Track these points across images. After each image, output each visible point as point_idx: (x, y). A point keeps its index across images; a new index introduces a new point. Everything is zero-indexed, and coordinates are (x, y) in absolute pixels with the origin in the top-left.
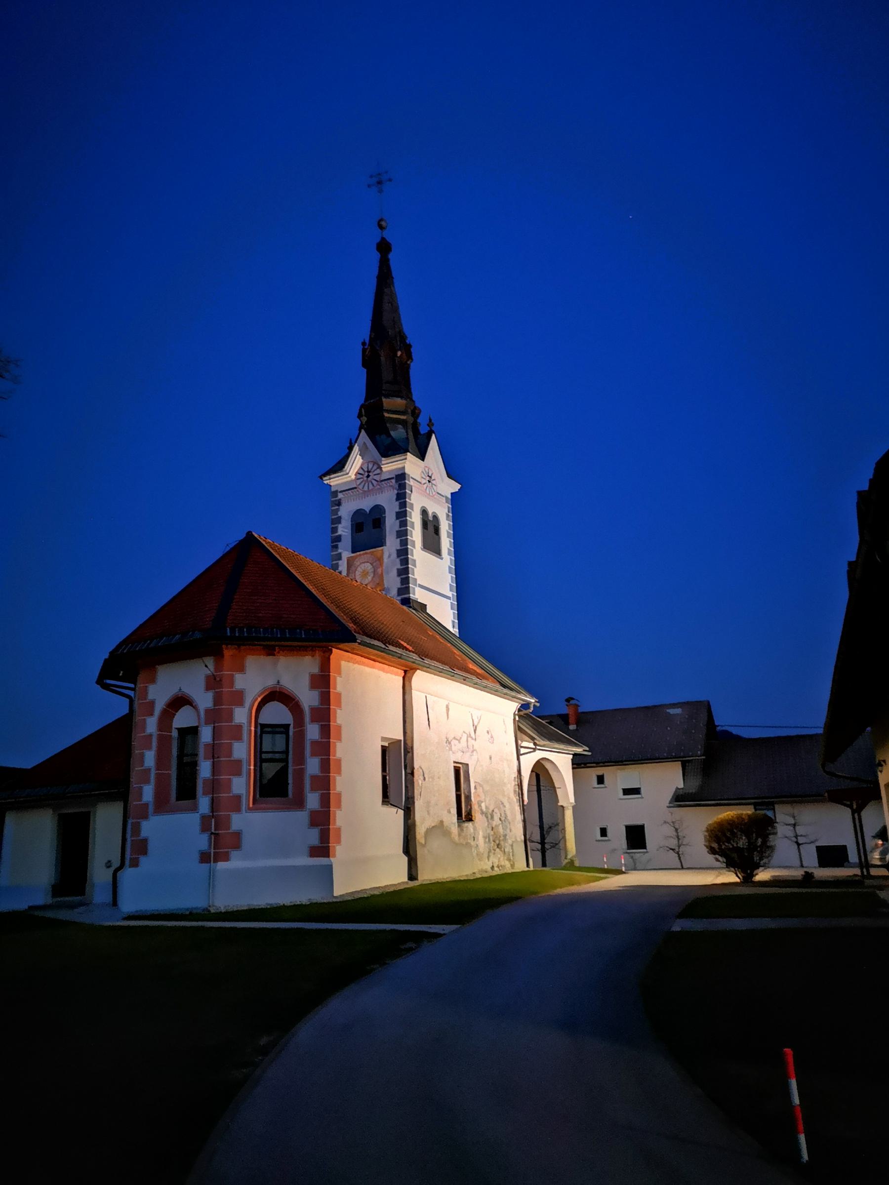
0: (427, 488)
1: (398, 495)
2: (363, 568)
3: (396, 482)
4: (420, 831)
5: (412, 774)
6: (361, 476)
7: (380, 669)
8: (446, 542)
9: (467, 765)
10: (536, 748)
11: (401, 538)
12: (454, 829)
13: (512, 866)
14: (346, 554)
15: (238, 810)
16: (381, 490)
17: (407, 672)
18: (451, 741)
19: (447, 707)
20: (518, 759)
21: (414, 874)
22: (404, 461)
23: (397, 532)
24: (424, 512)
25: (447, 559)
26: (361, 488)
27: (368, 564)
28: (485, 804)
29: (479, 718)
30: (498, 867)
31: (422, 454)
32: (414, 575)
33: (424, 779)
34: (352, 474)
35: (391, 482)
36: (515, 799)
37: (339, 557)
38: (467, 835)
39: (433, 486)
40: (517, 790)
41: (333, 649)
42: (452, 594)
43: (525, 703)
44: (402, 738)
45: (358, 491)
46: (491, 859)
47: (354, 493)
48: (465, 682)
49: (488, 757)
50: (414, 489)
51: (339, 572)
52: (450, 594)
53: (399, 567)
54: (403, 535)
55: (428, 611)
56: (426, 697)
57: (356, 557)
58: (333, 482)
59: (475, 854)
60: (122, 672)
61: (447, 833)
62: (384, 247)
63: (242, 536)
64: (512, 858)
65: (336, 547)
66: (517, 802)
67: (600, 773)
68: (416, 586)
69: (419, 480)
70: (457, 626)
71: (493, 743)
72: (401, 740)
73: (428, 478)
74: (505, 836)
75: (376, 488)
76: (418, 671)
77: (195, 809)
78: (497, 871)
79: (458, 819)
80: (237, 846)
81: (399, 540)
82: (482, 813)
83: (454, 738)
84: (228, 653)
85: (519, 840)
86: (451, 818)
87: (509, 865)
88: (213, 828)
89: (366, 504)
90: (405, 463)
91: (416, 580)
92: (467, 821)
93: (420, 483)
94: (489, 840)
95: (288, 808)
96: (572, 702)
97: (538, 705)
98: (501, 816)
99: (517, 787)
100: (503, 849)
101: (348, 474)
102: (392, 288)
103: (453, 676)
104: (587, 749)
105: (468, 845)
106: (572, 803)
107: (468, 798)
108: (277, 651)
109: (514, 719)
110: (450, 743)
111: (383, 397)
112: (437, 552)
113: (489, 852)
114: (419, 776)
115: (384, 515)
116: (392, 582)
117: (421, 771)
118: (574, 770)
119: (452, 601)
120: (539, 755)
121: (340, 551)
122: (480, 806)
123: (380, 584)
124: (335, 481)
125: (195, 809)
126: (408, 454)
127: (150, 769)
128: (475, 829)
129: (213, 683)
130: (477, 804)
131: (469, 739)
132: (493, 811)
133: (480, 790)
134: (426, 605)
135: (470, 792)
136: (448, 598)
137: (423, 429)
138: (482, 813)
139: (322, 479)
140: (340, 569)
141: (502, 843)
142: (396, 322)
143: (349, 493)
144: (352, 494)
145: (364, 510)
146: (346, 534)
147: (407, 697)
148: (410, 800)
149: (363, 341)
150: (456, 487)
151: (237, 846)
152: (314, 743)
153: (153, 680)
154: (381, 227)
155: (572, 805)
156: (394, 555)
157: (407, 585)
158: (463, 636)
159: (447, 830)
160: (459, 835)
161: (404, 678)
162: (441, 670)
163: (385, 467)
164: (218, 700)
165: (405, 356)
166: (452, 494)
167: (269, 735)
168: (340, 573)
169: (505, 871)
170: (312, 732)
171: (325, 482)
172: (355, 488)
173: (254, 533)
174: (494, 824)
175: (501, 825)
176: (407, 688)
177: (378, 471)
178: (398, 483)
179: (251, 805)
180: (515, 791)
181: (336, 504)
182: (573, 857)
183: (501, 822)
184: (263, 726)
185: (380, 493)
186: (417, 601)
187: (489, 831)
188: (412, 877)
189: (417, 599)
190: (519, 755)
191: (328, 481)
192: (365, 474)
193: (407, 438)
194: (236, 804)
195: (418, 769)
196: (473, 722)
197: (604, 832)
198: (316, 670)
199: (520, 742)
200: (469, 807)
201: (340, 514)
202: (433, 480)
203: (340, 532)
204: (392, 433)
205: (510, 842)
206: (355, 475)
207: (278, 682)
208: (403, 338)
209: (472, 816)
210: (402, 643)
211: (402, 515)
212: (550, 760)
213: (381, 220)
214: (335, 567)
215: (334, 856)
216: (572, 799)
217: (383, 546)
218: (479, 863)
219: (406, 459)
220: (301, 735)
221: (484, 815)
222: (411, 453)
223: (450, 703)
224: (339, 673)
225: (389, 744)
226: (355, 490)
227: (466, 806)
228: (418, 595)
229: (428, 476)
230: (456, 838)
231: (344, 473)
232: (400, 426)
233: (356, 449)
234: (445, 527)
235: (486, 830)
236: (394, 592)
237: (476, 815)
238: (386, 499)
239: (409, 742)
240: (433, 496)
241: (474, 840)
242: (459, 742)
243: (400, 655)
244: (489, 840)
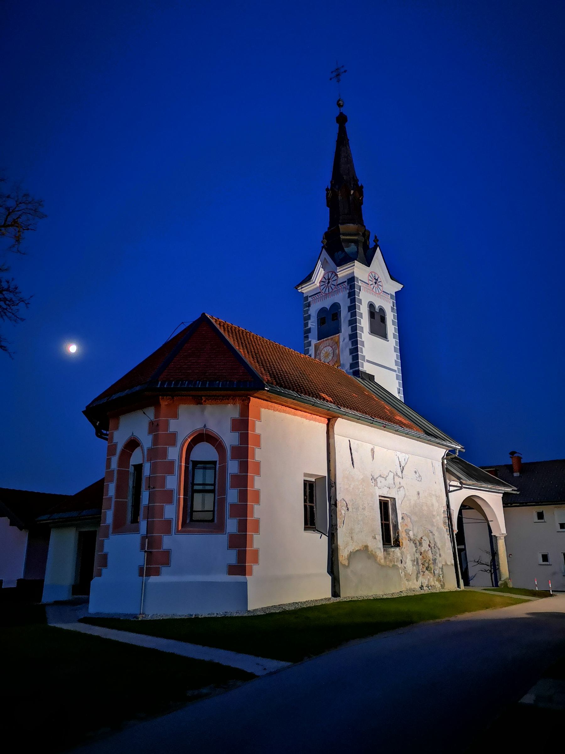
0: (373, 287)
1: (349, 293)
2: (326, 351)
3: (348, 284)
4: (343, 554)
5: (336, 505)
6: (324, 283)
7: (302, 416)
8: (391, 329)
9: (395, 499)
10: (462, 486)
11: (352, 326)
12: (380, 554)
13: (443, 586)
14: (314, 342)
15: (168, 532)
16: (338, 292)
17: (331, 420)
18: (377, 478)
19: (373, 450)
20: (447, 496)
21: (337, 591)
22: (353, 267)
23: (349, 321)
24: (371, 306)
25: (392, 342)
26: (324, 292)
27: (330, 347)
28: (413, 532)
29: (406, 461)
30: (427, 586)
31: (368, 262)
32: (362, 353)
33: (348, 509)
34: (317, 283)
35: (344, 284)
36: (444, 529)
37: (309, 344)
38: (394, 559)
39: (379, 286)
40: (447, 521)
41: (251, 398)
42: (397, 368)
43: (451, 449)
44: (326, 475)
45: (321, 294)
46: (421, 579)
47: (319, 296)
48: (385, 428)
49: (416, 493)
51: (309, 355)
52: (395, 368)
53: (351, 347)
54: (353, 323)
55: (375, 381)
56: (349, 440)
57: (320, 343)
58: (303, 290)
59: (403, 575)
60: (98, 422)
61: (372, 556)
62: (342, 119)
63: (197, 316)
64: (442, 580)
65: (307, 337)
66: (447, 531)
67: (540, 511)
68: (365, 361)
70: (402, 392)
71: (421, 481)
72: (326, 476)
73: (374, 281)
74: (435, 560)
75: (334, 290)
76: (339, 418)
77: (137, 530)
78: (426, 590)
79: (383, 544)
80: (167, 563)
81: (350, 327)
82: (410, 540)
83: (380, 476)
84: (164, 403)
85: (449, 563)
86: (377, 544)
87: (439, 586)
88: (146, 549)
89: (327, 303)
90: (354, 268)
91: (364, 356)
92: (395, 546)
93: (368, 284)
94: (417, 563)
95: (211, 532)
96: (516, 455)
97: (464, 450)
98: (430, 542)
99: (447, 519)
100: (432, 572)
101: (314, 283)
102: (348, 147)
103: (372, 423)
104: (516, 489)
105: (395, 567)
106: (503, 534)
107: (396, 527)
108: (204, 400)
109: (443, 463)
110: (375, 480)
111: (339, 225)
112: (384, 336)
113: (417, 574)
114: (341, 507)
116: (346, 359)
117: (344, 502)
118: (504, 508)
119: (397, 373)
120: (465, 493)
121: (310, 339)
122: (407, 533)
123: (338, 361)
124: (306, 289)
125: (137, 530)
126: (356, 261)
127: (112, 497)
128: (402, 553)
129: (154, 427)
130: (404, 532)
131: (396, 477)
133: (407, 520)
134: (374, 376)
135: (397, 522)
136: (395, 371)
137: (371, 244)
138: (410, 540)
139: (297, 288)
140: (310, 353)
141: (432, 566)
142: (351, 171)
143: (315, 296)
144: (317, 297)
145: (326, 308)
146: (314, 327)
147: (331, 441)
148: (334, 527)
149: (327, 187)
150: (399, 287)
151: (167, 563)
152: (234, 476)
153: (117, 428)
154: (339, 105)
155: (504, 535)
156: (347, 339)
157: (357, 361)
158: (407, 402)
159: (372, 554)
160: (385, 558)
161: (328, 425)
162: (359, 418)
163: (340, 274)
164: (156, 441)
165: (357, 194)
166: (395, 292)
168: (310, 356)
169: (434, 591)
170: (233, 467)
171: (299, 291)
172: (320, 292)
173: (206, 314)
174: (423, 550)
175: (430, 551)
176: (331, 433)
177: (336, 277)
178: (349, 285)
179: (180, 528)
180: (445, 523)
181: (306, 306)
182: (507, 579)
183: (430, 548)
184: (195, 463)
185: (337, 294)
186: (366, 373)
187: (418, 555)
188: (335, 593)
189: (366, 371)
190: (447, 492)
191: (301, 290)
192: (326, 281)
193: (358, 252)
194: (167, 526)
195: (341, 501)
196: (400, 463)
197: (545, 558)
198: (236, 414)
199: (448, 481)
200: (397, 535)
201: (309, 313)
202: (379, 282)
203: (310, 326)
204: (346, 249)
205: (440, 565)
206: (320, 283)
207: (205, 426)
208: (356, 181)
209: (399, 542)
210: (323, 395)
211: (353, 309)
212: (481, 498)
213: (339, 100)
214: (306, 352)
215: (251, 574)
216: (504, 531)
217: (339, 333)
218: (406, 582)
219: (354, 265)
220: (224, 469)
221: (412, 542)
222: (358, 261)
223: (375, 446)
224: (259, 418)
225: (315, 479)
226: (320, 294)
227: (394, 533)
228: (366, 368)
229: (375, 279)
230: (382, 561)
231: (311, 282)
232: (353, 244)
233: (319, 263)
234: (391, 317)
235: (414, 555)
236: (348, 366)
237: (403, 541)
238: (341, 298)
239: (333, 479)
240: (379, 294)
241: (402, 563)
242: (386, 480)
243: (313, 403)
244: (417, 563)
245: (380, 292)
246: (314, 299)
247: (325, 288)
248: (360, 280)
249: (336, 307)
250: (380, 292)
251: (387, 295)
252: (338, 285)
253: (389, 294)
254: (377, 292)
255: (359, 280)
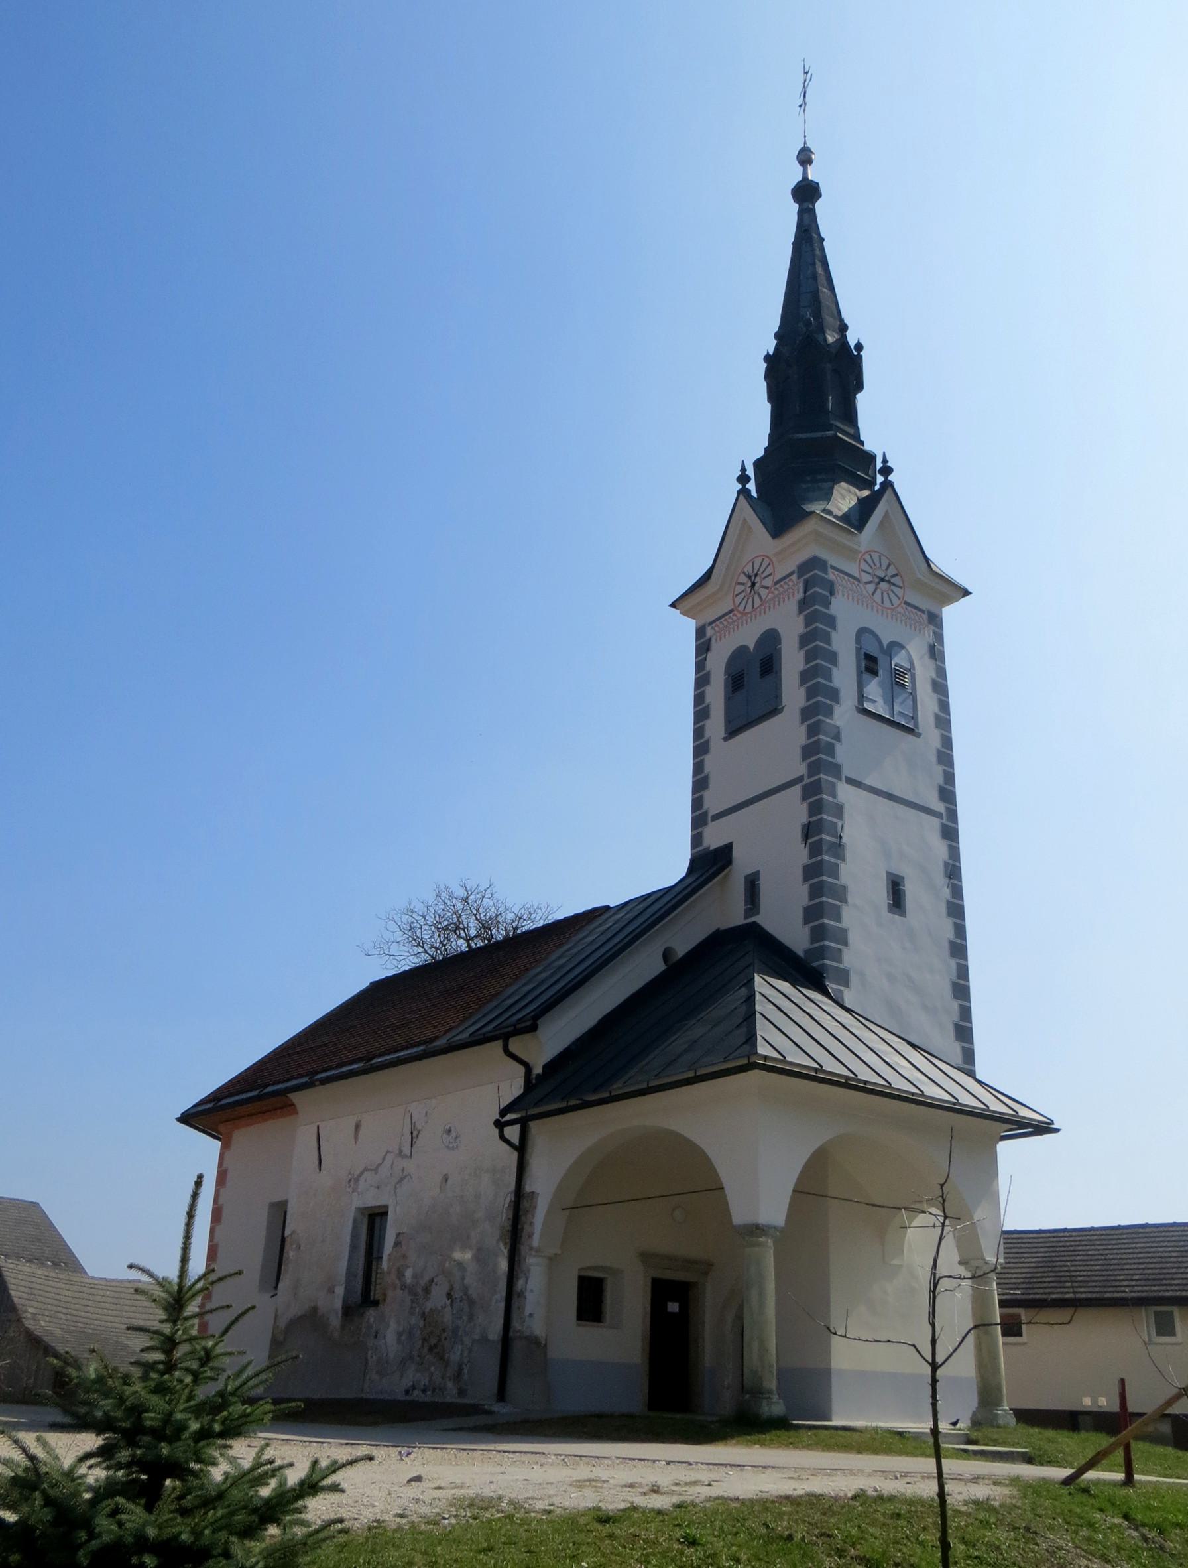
3: (799, 577)
13: (462, 1392)
50: (837, 588)
69: (857, 575)
93: (858, 580)
115: (143, 1501)
119: (944, 821)
132: (432, 1281)
149: (766, 353)
167: (496, 1042)
172: (731, 611)
175: (449, 1308)
221: (407, 1291)
245: (896, 604)
246: (717, 629)
247: (746, 599)
248: (833, 567)
249: (771, 639)
250: (896, 604)
251: (919, 613)
252: (777, 583)
253: (923, 611)
254: (887, 604)
255: (829, 567)
